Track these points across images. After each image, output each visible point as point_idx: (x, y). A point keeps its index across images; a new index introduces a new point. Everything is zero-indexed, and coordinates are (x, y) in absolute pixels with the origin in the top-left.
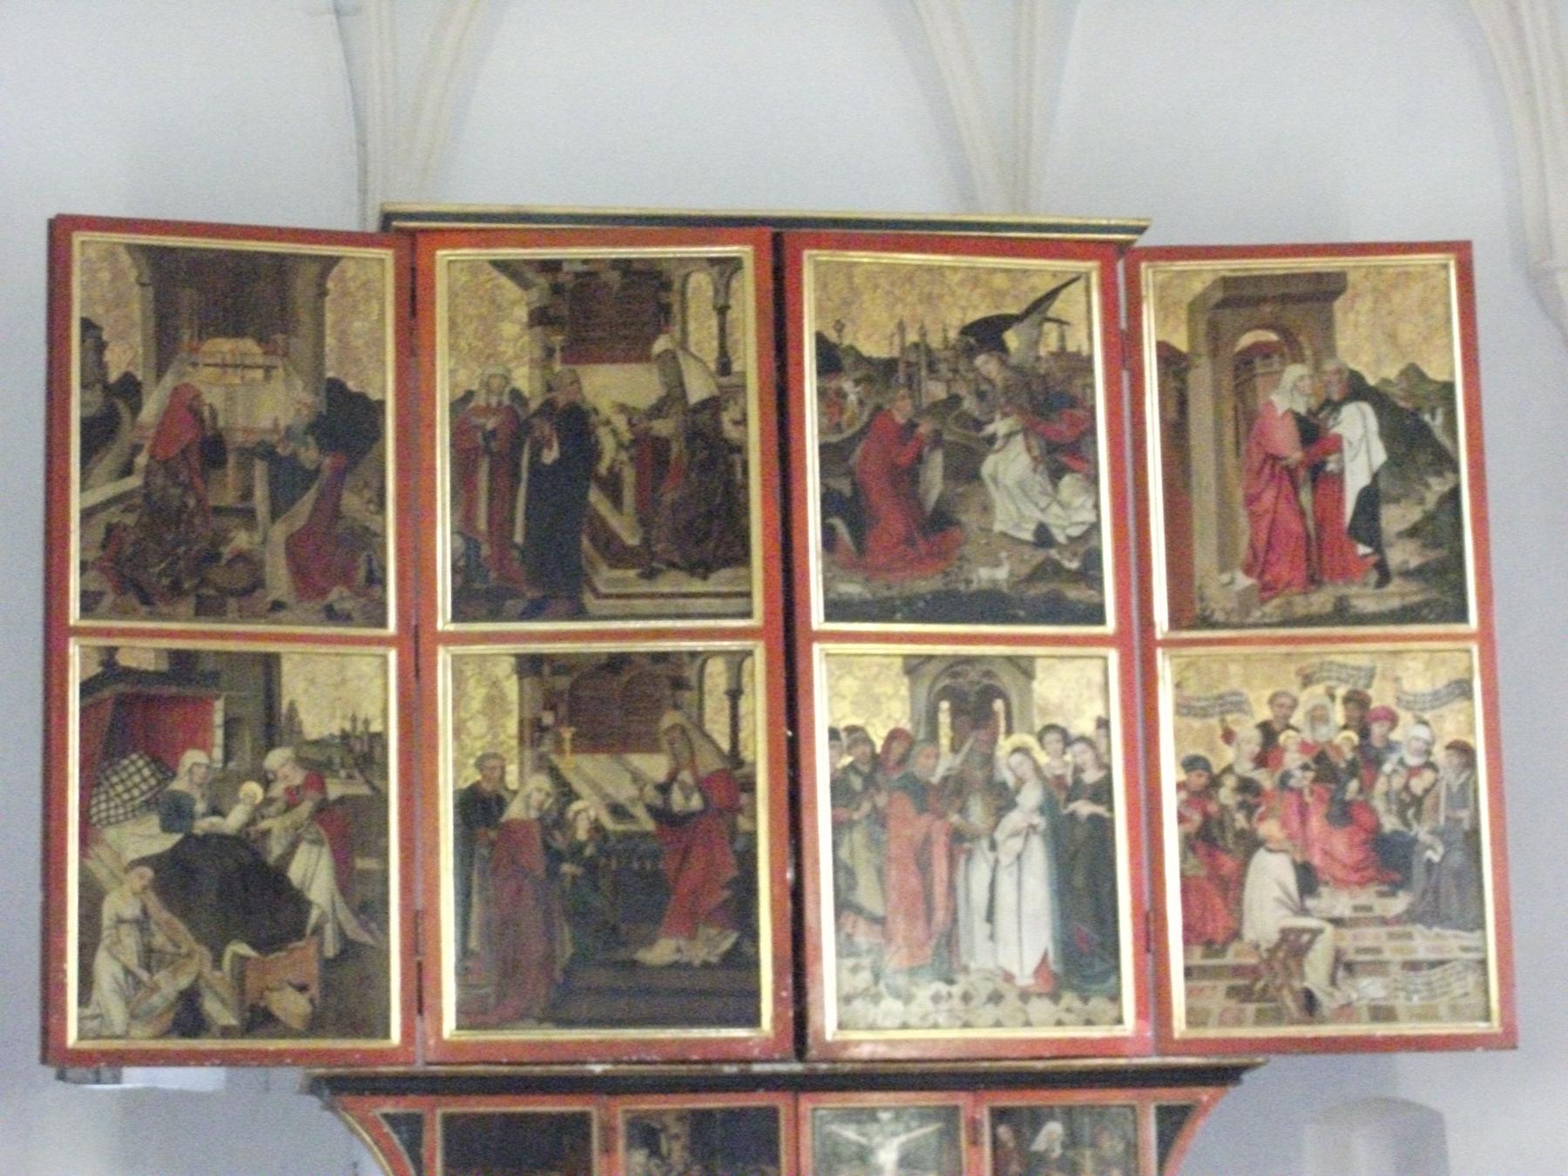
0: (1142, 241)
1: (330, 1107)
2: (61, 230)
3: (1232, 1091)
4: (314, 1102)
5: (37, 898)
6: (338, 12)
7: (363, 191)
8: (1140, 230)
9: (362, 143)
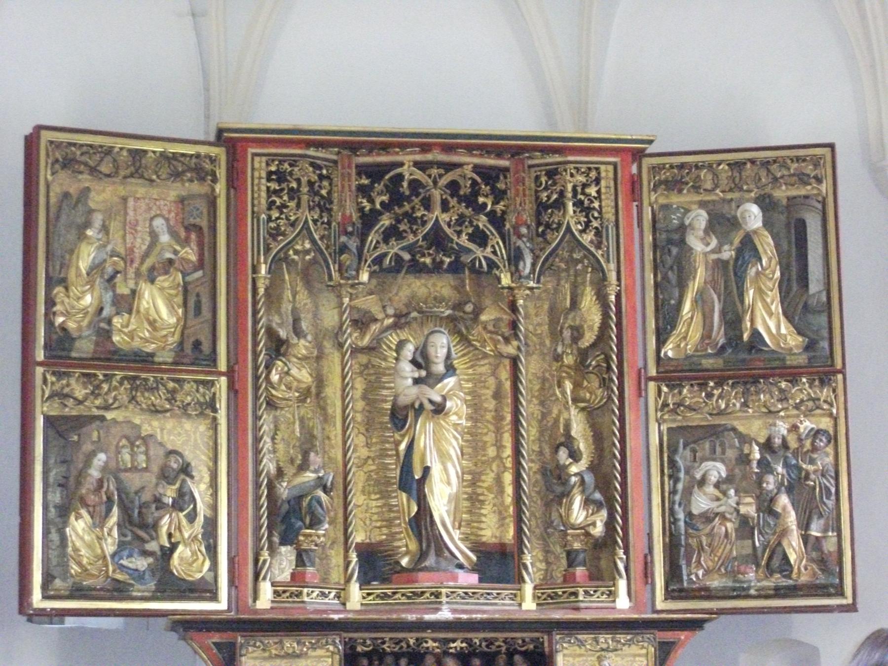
0: (651, 149)
1: (184, 639)
2: (31, 143)
3: (699, 634)
4: (174, 636)
5: (17, 520)
6: (193, 15)
7: (207, 117)
8: (650, 142)
9: (207, 90)
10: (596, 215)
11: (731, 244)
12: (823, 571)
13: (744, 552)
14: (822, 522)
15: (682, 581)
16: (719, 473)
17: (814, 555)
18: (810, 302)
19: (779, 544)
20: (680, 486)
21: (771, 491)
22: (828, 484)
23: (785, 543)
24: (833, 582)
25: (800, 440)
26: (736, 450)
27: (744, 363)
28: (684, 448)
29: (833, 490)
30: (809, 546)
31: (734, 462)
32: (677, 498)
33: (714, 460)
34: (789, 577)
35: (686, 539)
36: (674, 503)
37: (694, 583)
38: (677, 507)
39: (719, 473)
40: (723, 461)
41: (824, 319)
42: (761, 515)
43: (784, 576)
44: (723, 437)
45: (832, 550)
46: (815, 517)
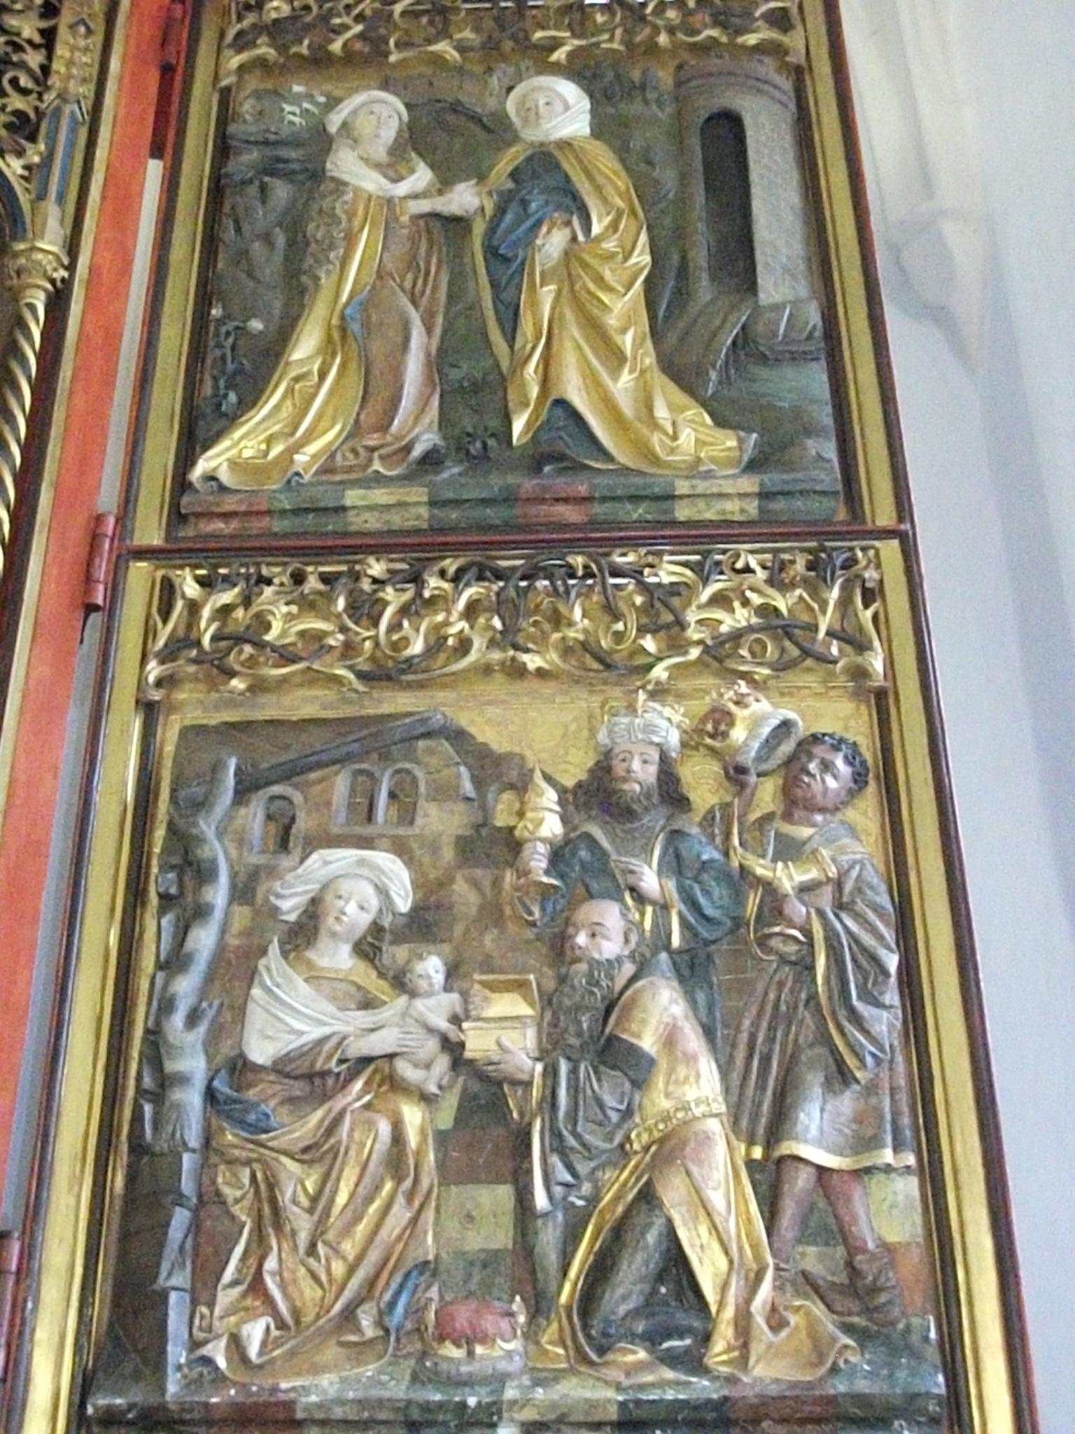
10: (24, 81)
11: (481, 178)
12: (863, 1337)
13: (475, 1242)
14: (846, 1103)
15: (157, 1363)
16: (383, 892)
17: (812, 1259)
18: (760, 328)
19: (648, 1197)
20: (203, 940)
21: (612, 965)
22: (868, 940)
23: (673, 1194)
24: (919, 1386)
25: (736, 774)
26: (461, 807)
27: (520, 514)
28: (243, 793)
29: (892, 962)
30: (789, 1211)
31: (448, 854)
32: (186, 986)
33: (366, 843)
34: (693, 1362)
35: (205, 1166)
36: (167, 1006)
37: (220, 1379)
38: (178, 1019)
39: (383, 892)
40: (401, 849)
41: (816, 379)
42: (564, 1067)
43: (672, 1360)
44: (411, 756)
45: (893, 1235)
46: (814, 1082)
